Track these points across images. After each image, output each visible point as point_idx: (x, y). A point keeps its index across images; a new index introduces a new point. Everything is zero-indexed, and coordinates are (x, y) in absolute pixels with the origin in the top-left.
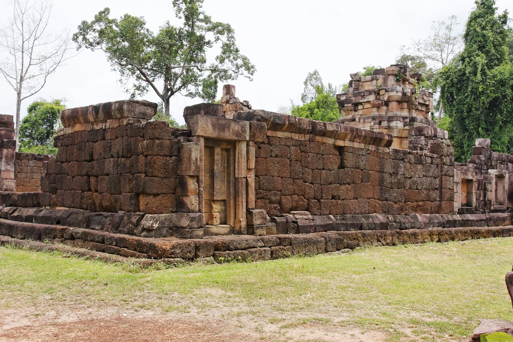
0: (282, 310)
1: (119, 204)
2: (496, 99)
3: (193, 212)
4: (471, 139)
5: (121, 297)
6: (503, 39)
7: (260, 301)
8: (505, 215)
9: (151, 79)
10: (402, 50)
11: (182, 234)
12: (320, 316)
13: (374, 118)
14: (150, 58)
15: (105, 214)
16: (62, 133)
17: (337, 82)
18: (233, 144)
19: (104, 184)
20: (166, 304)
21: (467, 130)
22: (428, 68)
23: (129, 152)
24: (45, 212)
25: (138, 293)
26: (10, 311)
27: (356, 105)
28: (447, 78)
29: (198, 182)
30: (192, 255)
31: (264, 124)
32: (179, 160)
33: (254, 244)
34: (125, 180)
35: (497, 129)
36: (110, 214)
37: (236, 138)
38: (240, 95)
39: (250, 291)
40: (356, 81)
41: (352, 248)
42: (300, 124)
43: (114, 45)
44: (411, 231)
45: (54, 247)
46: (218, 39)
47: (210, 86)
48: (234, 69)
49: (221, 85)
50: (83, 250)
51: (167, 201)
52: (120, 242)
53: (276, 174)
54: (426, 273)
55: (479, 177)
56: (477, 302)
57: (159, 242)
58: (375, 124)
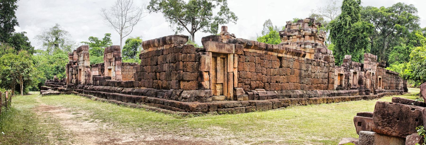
0: (251, 137)
1: (170, 86)
2: (355, 37)
3: (207, 89)
4: (343, 55)
5: (174, 130)
6: (359, 11)
7: (240, 133)
8: (357, 90)
9: (185, 24)
10: (312, 11)
11: (201, 100)
12: (269, 139)
13: (297, 43)
14: (184, 14)
15: (164, 90)
16: (143, 52)
17: (280, 25)
18: (226, 55)
19: (163, 76)
20: (195, 134)
21: (342, 51)
22: (324, 21)
23: (175, 60)
24: (136, 89)
25: (182, 128)
26: (124, 134)
27: (289, 36)
28: (333, 26)
29: (209, 74)
30: (206, 110)
31: (242, 45)
32: (200, 64)
33: (237, 105)
34: (173, 74)
35: (355, 51)
36: (166, 90)
37: (228, 52)
38: (230, 31)
39: (235, 128)
40: (289, 25)
41: (286, 107)
42: (260, 45)
43: (167, 9)
44: (314, 98)
45: (141, 106)
46: (218, 4)
47: (215, 27)
48: (227, 18)
49: (220, 26)
50: (154, 108)
51: (193, 84)
52: (172, 104)
53: (248, 70)
54: (320, 118)
55: (346, 73)
56: (342, 130)
57: (190, 104)
58: (298, 46)
